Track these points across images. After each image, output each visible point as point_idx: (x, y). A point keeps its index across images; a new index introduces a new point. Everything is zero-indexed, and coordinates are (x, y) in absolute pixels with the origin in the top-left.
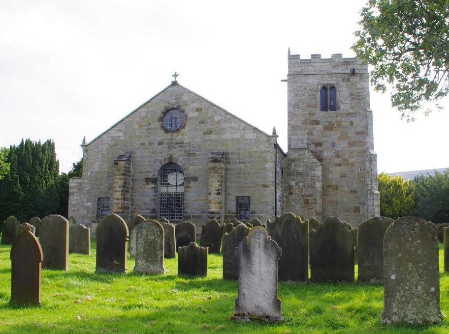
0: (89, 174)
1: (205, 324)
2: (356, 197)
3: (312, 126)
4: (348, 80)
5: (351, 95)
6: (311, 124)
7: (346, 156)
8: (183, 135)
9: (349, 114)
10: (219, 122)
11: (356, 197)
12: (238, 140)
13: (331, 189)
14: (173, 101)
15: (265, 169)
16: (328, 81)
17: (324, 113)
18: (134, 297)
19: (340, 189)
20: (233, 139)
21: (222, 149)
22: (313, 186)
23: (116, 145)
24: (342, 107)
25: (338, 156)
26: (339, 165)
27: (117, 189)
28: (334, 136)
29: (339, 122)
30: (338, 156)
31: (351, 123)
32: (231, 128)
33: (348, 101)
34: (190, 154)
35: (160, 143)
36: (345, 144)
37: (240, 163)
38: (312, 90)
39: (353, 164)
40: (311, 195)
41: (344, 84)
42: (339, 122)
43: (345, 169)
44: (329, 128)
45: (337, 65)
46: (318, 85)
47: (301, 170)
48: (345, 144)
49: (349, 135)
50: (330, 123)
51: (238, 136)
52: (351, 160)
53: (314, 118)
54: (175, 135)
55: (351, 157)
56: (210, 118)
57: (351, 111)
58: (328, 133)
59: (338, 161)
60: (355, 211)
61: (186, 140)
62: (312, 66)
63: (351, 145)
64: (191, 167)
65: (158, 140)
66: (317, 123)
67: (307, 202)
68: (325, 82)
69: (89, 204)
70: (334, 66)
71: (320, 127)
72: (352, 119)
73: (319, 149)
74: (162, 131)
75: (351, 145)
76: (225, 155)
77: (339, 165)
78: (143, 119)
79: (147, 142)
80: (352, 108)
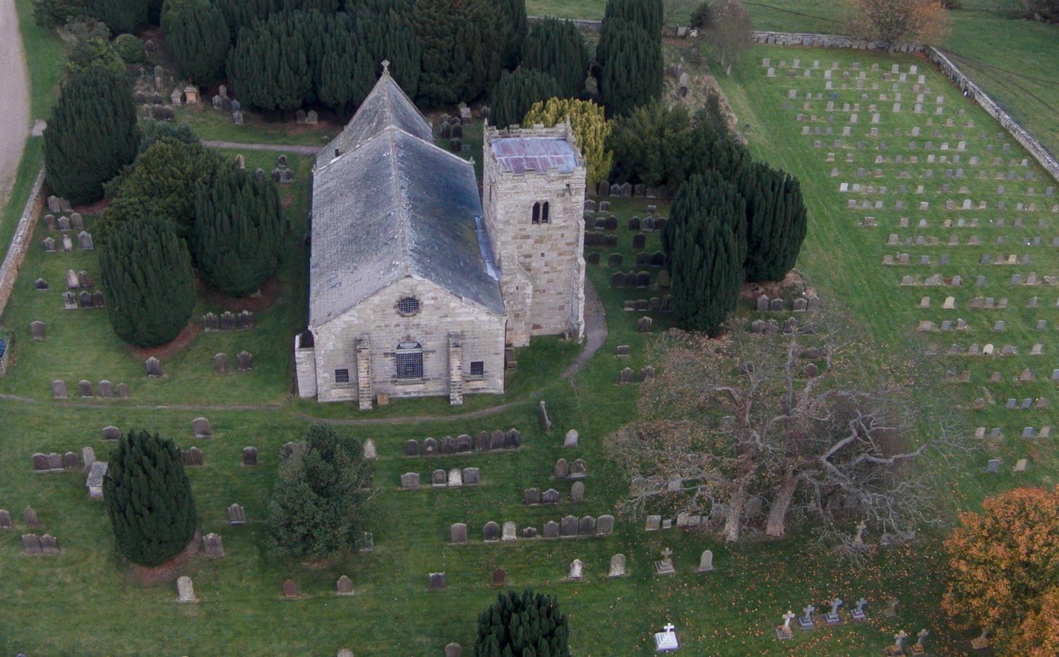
0: (323, 352)
1: (529, 528)
2: (562, 298)
3: (522, 241)
4: (563, 195)
5: (565, 209)
6: (522, 238)
7: (554, 266)
8: (420, 318)
9: (561, 227)
10: (454, 308)
11: (562, 298)
12: (472, 321)
13: (538, 293)
14: (408, 292)
15: (497, 342)
16: (542, 198)
17: (536, 226)
18: (117, 189)
19: (546, 292)
20: (467, 322)
21: (458, 330)
22: (523, 303)
23: (350, 327)
24: (554, 221)
25: (546, 265)
26: (548, 272)
27: (363, 370)
28: (544, 248)
29: (551, 236)
30: (546, 265)
31: (563, 236)
32: (466, 313)
33: (561, 216)
34: (426, 333)
35: (397, 325)
36: (555, 254)
37: (474, 338)
38: (524, 207)
39: (560, 271)
40: (522, 310)
41: (559, 200)
42: (551, 236)
43: (553, 275)
44: (539, 241)
45: (553, 181)
46: (531, 202)
47: (512, 290)
48: (555, 254)
49: (558, 246)
50: (541, 237)
51: (472, 318)
52: (559, 268)
53: (525, 233)
54: (411, 319)
55: (559, 265)
56: (445, 305)
57: (563, 224)
58: (538, 245)
59: (546, 269)
60: (560, 309)
61: (423, 322)
62: (525, 182)
63: (560, 254)
64: (429, 343)
65: (395, 323)
66: (527, 237)
67: (517, 316)
68: (539, 199)
69: (326, 375)
70: (549, 182)
71: (531, 241)
72: (564, 232)
73: (528, 260)
74: (398, 316)
75: (560, 254)
76: (461, 336)
77: (548, 272)
78: (377, 306)
79: (383, 325)
80: (565, 221)
